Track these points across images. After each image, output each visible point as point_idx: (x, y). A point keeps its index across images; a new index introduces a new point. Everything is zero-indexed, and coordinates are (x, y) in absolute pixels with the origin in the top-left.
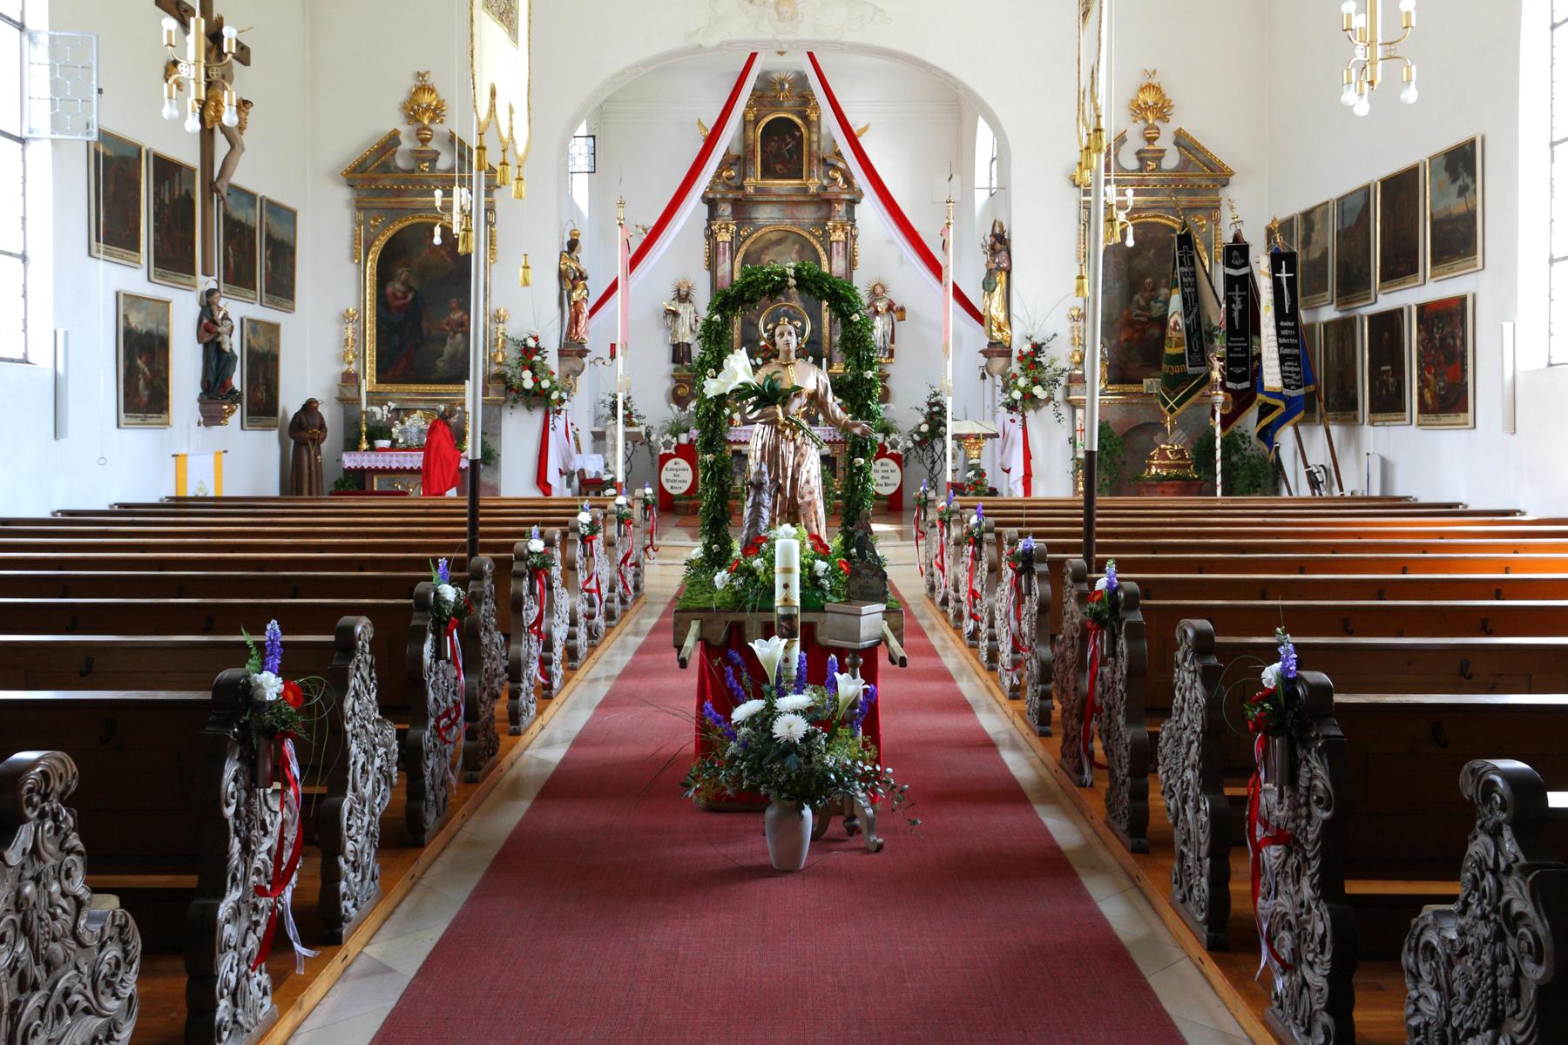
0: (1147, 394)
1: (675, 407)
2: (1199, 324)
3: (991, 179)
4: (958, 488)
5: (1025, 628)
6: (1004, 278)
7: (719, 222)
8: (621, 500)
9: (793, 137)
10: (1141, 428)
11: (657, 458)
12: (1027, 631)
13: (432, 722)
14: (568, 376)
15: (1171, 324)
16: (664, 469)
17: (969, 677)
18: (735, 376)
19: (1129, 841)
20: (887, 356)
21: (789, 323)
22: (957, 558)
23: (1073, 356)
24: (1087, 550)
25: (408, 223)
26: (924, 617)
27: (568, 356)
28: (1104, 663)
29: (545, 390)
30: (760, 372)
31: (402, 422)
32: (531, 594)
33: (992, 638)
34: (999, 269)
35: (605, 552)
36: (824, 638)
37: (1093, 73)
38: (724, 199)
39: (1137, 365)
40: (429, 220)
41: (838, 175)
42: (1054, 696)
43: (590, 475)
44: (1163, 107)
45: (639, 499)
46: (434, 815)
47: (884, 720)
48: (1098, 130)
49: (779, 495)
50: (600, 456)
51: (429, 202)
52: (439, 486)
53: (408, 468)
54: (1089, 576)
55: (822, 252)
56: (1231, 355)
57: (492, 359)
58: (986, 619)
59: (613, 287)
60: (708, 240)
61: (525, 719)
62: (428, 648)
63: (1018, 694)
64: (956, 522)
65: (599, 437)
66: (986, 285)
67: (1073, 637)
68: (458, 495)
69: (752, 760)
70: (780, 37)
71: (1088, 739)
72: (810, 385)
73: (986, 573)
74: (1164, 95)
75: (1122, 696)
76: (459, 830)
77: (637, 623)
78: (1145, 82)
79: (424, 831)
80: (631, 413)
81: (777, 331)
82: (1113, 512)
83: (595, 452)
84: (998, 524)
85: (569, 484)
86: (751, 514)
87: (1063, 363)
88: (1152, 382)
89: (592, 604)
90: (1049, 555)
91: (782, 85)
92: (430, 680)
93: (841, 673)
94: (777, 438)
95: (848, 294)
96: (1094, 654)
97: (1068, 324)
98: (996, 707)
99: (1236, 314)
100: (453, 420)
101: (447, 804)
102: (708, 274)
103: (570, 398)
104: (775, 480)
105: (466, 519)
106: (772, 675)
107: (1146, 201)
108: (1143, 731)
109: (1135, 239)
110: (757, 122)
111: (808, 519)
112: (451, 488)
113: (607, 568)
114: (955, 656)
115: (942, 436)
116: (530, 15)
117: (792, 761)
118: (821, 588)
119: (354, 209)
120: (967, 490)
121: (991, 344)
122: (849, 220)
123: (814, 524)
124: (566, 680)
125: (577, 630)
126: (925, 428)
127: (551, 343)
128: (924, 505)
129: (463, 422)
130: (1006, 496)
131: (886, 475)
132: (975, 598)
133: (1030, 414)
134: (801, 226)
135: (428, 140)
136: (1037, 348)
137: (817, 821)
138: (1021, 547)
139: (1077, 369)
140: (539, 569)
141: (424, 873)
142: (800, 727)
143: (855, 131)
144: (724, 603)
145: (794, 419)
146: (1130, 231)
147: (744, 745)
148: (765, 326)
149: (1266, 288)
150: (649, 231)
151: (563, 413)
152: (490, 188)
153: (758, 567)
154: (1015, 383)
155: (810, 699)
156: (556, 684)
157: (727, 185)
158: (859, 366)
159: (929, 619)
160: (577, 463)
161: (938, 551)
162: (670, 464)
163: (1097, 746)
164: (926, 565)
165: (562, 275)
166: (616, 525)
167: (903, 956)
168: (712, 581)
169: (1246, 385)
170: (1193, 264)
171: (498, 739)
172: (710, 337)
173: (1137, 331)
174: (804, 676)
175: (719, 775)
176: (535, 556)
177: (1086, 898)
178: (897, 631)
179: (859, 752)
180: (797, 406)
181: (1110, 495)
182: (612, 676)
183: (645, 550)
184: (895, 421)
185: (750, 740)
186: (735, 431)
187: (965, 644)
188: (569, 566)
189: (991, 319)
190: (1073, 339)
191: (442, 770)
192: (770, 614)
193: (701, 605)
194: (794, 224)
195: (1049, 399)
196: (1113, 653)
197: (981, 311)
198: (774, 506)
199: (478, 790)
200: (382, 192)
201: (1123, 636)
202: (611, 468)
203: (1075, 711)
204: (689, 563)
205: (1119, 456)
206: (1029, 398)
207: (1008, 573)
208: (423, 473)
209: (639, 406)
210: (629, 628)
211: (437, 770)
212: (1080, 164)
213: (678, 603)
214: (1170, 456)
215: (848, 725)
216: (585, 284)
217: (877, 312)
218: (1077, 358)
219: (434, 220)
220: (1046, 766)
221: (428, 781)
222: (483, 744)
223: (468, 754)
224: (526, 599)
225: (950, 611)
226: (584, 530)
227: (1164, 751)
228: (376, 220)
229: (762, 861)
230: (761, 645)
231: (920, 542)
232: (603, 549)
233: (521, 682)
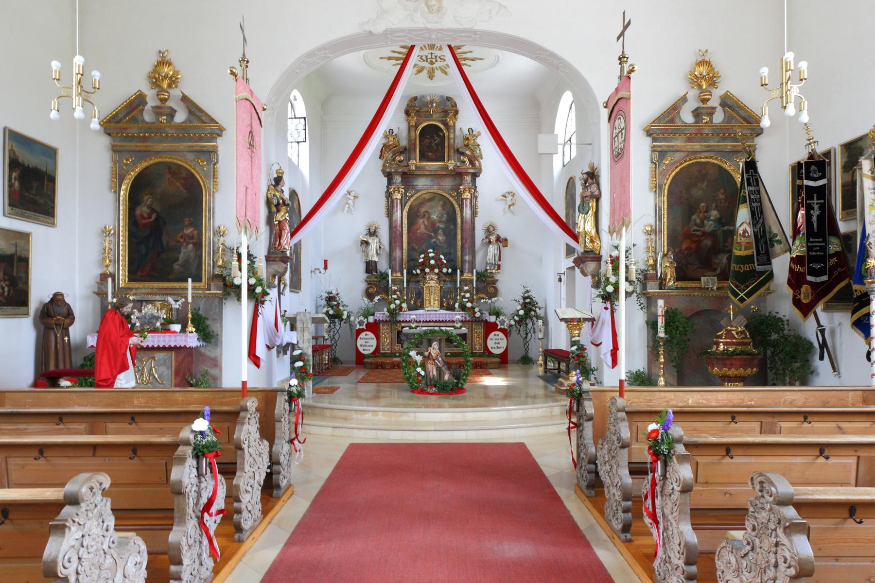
1: (366, 299)
2: (764, 231)
9: (438, 136)
11: (354, 331)
15: (741, 231)
16: (359, 338)
20: (496, 268)
25: (152, 162)
27: (273, 261)
38: (396, 172)
41: (466, 159)
44: (713, 77)
55: (456, 206)
56: (811, 253)
60: (387, 199)
70: (429, 26)
74: (714, 69)
78: (700, 59)
88: (708, 280)
97: (644, 237)
99: (814, 219)
110: (416, 127)
119: (112, 152)
126: (522, 312)
131: (497, 341)
135: (166, 100)
149: (869, 189)
157: (398, 165)
162: (363, 335)
169: (824, 278)
170: (758, 185)
173: (695, 242)
184: (502, 308)
190: (648, 248)
194: (439, 189)
200: (132, 138)
214: (736, 336)
217: (490, 242)
218: (651, 262)
228: (127, 160)
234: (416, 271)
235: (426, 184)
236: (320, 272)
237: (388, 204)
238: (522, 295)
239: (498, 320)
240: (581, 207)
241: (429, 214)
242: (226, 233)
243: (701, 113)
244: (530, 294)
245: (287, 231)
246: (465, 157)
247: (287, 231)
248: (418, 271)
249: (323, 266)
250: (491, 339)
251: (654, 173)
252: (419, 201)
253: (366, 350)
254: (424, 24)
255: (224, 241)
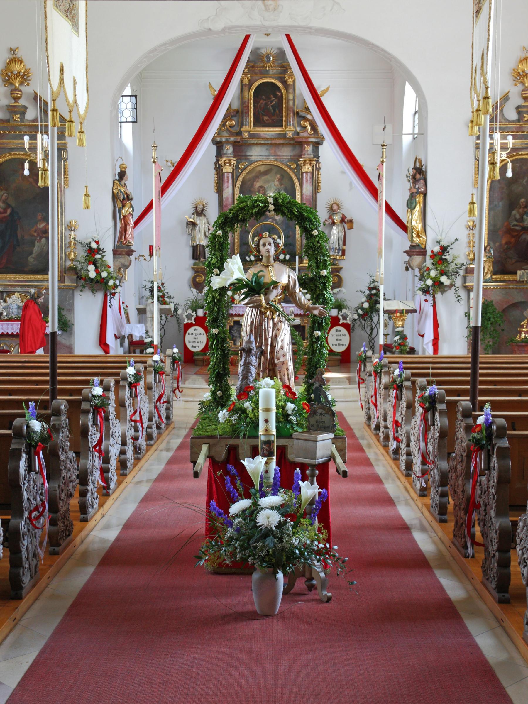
0: (520, 282)
3: (414, 127)
4: (387, 348)
5: (430, 448)
6: (421, 199)
7: (224, 158)
8: (156, 357)
9: (276, 96)
10: (515, 305)
11: (182, 326)
12: (431, 450)
13: (26, 514)
14: (120, 269)
17: (393, 480)
18: (232, 274)
19: (497, 595)
20: (340, 254)
21: (269, 236)
22: (386, 397)
23: (469, 255)
24: (473, 394)
25: (6, 158)
26: (363, 438)
27: (120, 254)
28: (482, 475)
29: (104, 279)
30: (249, 271)
31: (5, 301)
32: (94, 425)
33: (409, 454)
34: (418, 193)
35: (146, 394)
36: (292, 456)
37: (483, 55)
38: (227, 142)
39: (513, 261)
40: (21, 157)
41: (307, 124)
42: (449, 494)
43: (136, 338)
45: (169, 356)
46: (29, 577)
47: (332, 510)
48: (486, 98)
49: (262, 357)
50: (143, 325)
51: (19, 143)
52: (31, 346)
53: (10, 333)
54: (474, 413)
55: (295, 180)
57: (67, 256)
58: (404, 441)
59: (150, 207)
60: (217, 171)
61: (91, 511)
62: (23, 464)
63: (425, 493)
64: (386, 373)
65: (142, 312)
66: (409, 206)
67: (462, 455)
68: (45, 353)
69: (243, 540)
70: (267, 23)
71: (470, 525)
72: (284, 281)
73: (405, 409)
75: (494, 497)
76: (47, 587)
77: (168, 442)
78: (524, 56)
79: (21, 588)
80: (164, 295)
81: (261, 242)
82: (492, 364)
83: (140, 322)
84: (413, 375)
85: (122, 345)
86: (243, 370)
87: (462, 260)
88: (523, 273)
89: (136, 430)
90: (447, 398)
91: (268, 58)
92: (25, 486)
93: (303, 481)
94: (261, 317)
95: (310, 216)
96: (475, 467)
98: (411, 501)
100: (41, 300)
101: (38, 569)
102: (216, 196)
103: (122, 284)
104: (259, 347)
105: (48, 371)
106: (257, 483)
107: (522, 143)
108: (507, 521)
109: (513, 171)
111: (282, 374)
112: (39, 348)
113: (147, 405)
114: (384, 466)
115: (377, 311)
116: (86, 11)
117: (270, 541)
118: (290, 422)
120: (394, 349)
121: (412, 247)
122: (314, 157)
123: (286, 377)
124: (119, 483)
125: (126, 448)
126: (366, 305)
127: (108, 246)
128: (364, 360)
129: (47, 300)
130: (421, 354)
131: (339, 338)
132: (397, 426)
133: (438, 296)
134: (281, 161)
135: (19, 98)
136: (444, 249)
137: (287, 580)
138: (428, 392)
139: (471, 264)
140: (100, 407)
141: (22, 617)
142: (275, 518)
143: (319, 92)
144: (225, 432)
145: (273, 304)
146: (510, 165)
147: (238, 530)
148: (253, 239)
150: (175, 165)
151: (117, 295)
152: (61, 136)
153: (248, 407)
154: (429, 274)
155: (282, 499)
156: (112, 485)
157: (230, 131)
158: (318, 267)
159: (366, 439)
160: (127, 330)
161: (373, 393)
162: (191, 330)
163: (477, 530)
164: (365, 402)
165: (115, 197)
166: (153, 375)
167: (343, 674)
168: (217, 417)
171: (72, 525)
172: (215, 246)
174: (279, 483)
175: (221, 551)
176: (97, 399)
177: (468, 634)
178: (341, 451)
179: (315, 535)
180: (275, 294)
181: (493, 353)
182: (151, 480)
183: (174, 391)
185: (242, 527)
186: (236, 307)
187: (390, 457)
188: (121, 404)
189: (413, 228)
190: (469, 242)
191: (34, 547)
192: (255, 440)
193: (209, 434)
194: (276, 160)
195: (452, 285)
196: (489, 468)
197: (405, 223)
198: (259, 365)
199: (59, 559)
201: (495, 456)
202: (150, 334)
203: (462, 506)
204: (202, 403)
205: (500, 325)
206: (438, 284)
207: (419, 410)
208: (20, 336)
209: (169, 290)
210: (163, 446)
211: (30, 547)
212: (472, 122)
213: (193, 432)
215: (308, 516)
216: (131, 204)
217: (334, 223)
219: (24, 157)
220: (442, 542)
221: (24, 555)
222: (62, 528)
223: (51, 536)
224: (91, 428)
225: (381, 434)
226: (131, 379)
227: (521, 535)
229: (249, 608)
230: (249, 462)
231: (361, 385)
232: (144, 392)
233: (88, 485)
234: (249, 257)
235: (262, 154)
236: (145, 259)
237: (217, 177)
238: (368, 285)
239: (341, 313)
240: (409, 202)
241: (264, 189)
242: (77, 227)
243: (522, 111)
244: (376, 284)
245: (131, 225)
246: (306, 122)
247: (131, 225)
248: (252, 258)
249: (147, 253)
250: (333, 336)
251: (477, 169)
252: (253, 175)
253: (195, 347)
254: (261, 21)
255: (75, 235)
